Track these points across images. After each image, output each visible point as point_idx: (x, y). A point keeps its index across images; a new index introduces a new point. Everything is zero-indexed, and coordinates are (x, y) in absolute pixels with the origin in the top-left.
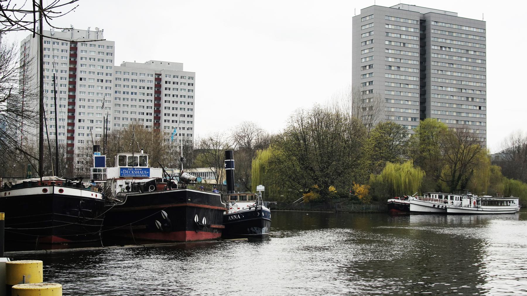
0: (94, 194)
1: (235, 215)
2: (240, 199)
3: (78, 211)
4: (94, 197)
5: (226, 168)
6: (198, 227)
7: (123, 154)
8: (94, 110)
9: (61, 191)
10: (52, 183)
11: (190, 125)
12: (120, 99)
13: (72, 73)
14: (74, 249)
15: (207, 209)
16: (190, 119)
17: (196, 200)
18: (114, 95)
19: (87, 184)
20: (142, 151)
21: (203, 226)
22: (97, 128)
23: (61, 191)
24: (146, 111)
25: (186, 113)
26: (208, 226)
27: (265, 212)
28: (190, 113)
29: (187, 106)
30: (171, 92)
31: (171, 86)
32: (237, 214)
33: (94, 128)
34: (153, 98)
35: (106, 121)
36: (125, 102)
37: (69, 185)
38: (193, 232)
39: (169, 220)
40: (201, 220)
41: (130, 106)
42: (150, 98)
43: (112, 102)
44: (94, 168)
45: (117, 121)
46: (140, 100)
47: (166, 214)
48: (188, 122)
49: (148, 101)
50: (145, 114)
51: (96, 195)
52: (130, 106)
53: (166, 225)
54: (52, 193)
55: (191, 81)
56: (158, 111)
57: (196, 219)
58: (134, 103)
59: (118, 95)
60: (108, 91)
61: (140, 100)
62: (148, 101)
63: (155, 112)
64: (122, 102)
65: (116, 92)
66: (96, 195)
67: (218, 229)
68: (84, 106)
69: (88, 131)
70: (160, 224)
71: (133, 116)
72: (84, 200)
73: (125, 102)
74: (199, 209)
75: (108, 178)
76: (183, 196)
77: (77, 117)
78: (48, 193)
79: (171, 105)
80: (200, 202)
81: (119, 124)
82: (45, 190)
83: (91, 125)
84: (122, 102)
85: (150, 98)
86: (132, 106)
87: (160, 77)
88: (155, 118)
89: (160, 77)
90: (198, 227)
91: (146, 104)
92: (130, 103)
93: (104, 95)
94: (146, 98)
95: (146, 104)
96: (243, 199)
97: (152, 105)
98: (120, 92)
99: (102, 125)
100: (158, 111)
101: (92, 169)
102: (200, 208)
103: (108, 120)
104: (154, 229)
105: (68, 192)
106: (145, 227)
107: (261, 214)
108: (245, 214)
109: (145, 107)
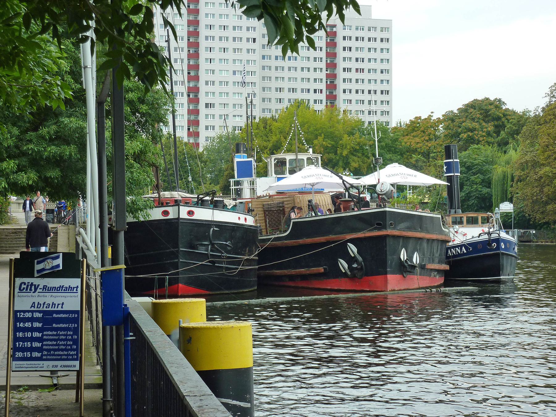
0: (243, 217)
1: (457, 246)
2: (483, 223)
3: (209, 245)
4: (242, 222)
5: (446, 173)
6: (405, 269)
7: (280, 156)
8: (230, 89)
9: (190, 213)
10: (176, 201)
11: (385, 108)
12: (270, 68)
13: (191, 29)
14: (463, 288)
15: (420, 239)
16: (385, 97)
17: (402, 225)
18: (260, 63)
19: (229, 202)
20: (311, 150)
21: (413, 267)
22: (234, 116)
23: (190, 213)
24: (313, 86)
25: (379, 87)
26: (422, 267)
27: (506, 242)
28: (385, 87)
29: (379, 76)
30: (354, 54)
31: (353, 44)
32: (460, 246)
33: (231, 116)
34: (323, 65)
35: (250, 105)
36: (280, 74)
37: (201, 203)
38: (398, 276)
39: (360, 259)
40: (410, 258)
41: (286, 79)
42: (319, 65)
43: (257, 73)
44: (236, 179)
45: (267, 105)
46: (302, 69)
47: (355, 249)
48: (382, 102)
49: (315, 69)
50: (312, 91)
51: (246, 219)
52: (286, 79)
53: (355, 266)
54: (177, 217)
55: (384, 35)
56: (332, 86)
57: (403, 255)
58: (293, 74)
59: (267, 62)
60: (251, 56)
61: (302, 69)
62: (315, 69)
63: (328, 87)
64: (273, 74)
65: (263, 57)
66: (246, 219)
67: (439, 271)
68: (213, 82)
69: (221, 122)
70: (346, 266)
71: (293, 96)
72: (217, 226)
73: (280, 74)
74: (407, 239)
75: (258, 195)
76: (380, 220)
77: (203, 99)
78: (171, 216)
79: (353, 75)
80: (409, 229)
81: (270, 110)
82: (166, 213)
83: (224, 112)
84: (273, 74)
85: (319, 65)
86: (290, 78)
87: (334, 29)
88: (328, 97)
89: (334, 29)
90: (405, 269)
91: (312, 75)
92: (286, 74)
93: (244, 62)
94: (312, 65)
95: (312, 75)
96: (473, 222)
97: (323, 75)
98: (270, 56)
99: (243, 112)
100: (332, 86)
101: (232, 180)
102: (408, 238)
103: (254, 103)
104: (337, 273)
105: (203, 214)
106: (321, 270)
107: (498, 247)
108: (474, 246)
109: (312, 80)
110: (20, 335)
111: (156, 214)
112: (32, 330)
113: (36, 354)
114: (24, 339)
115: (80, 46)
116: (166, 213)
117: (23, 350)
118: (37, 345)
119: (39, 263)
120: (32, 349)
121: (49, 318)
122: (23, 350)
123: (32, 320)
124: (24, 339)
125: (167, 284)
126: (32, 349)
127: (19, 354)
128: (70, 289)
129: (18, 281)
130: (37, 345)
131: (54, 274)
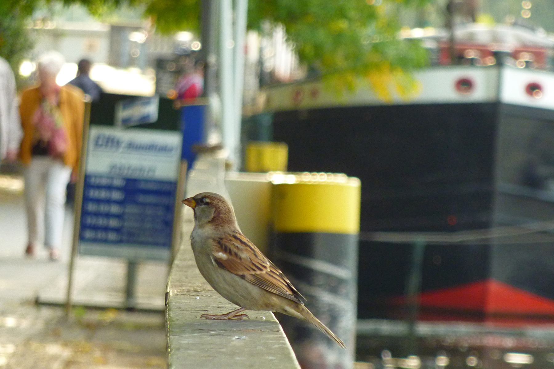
23: (533, 88)
82: (465, 84)
110: (91, 207)
111: (437, 87)
112: (108, 201)
113: (112, 236)
114: (97, 214)
115: (182, 108)
116: (465, 84)
117: (95, 228)
118: (113, 223)
119: (125, 107)
120: (106, 229)
121: (133, 188)
122: (95, 228)
123: (109, 188)
124: (97, 214)
125: (414, 281)
126: (106, 229)
127: (89, 234)
128: (164, 149)
129: (95, 132)
130: (113, 223)
131: (144, 125)
